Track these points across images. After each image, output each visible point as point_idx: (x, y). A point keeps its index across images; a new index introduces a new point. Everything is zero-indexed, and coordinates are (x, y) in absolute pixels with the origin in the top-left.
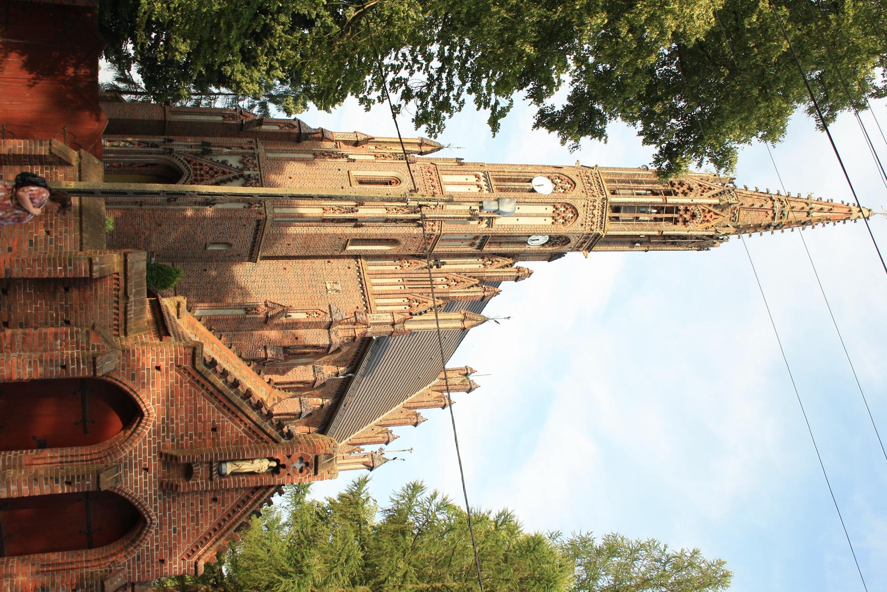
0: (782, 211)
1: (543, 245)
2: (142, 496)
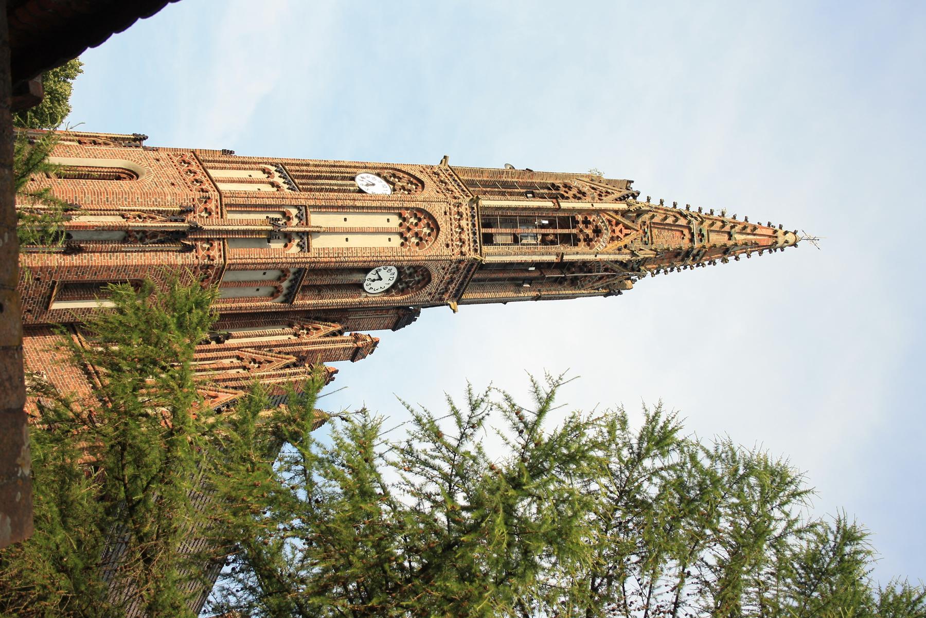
0: (701, 230)
1: (388, 292)
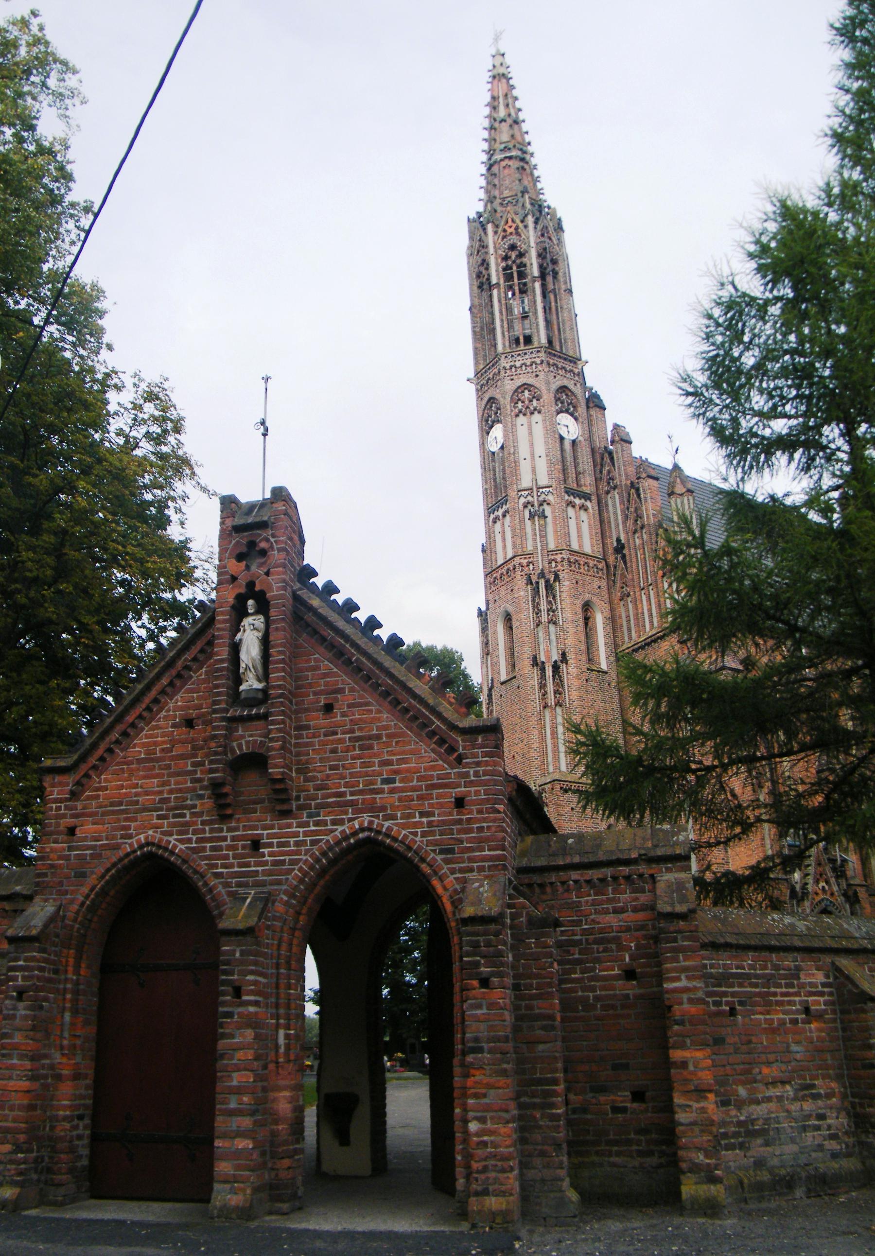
2: (307, 851)
